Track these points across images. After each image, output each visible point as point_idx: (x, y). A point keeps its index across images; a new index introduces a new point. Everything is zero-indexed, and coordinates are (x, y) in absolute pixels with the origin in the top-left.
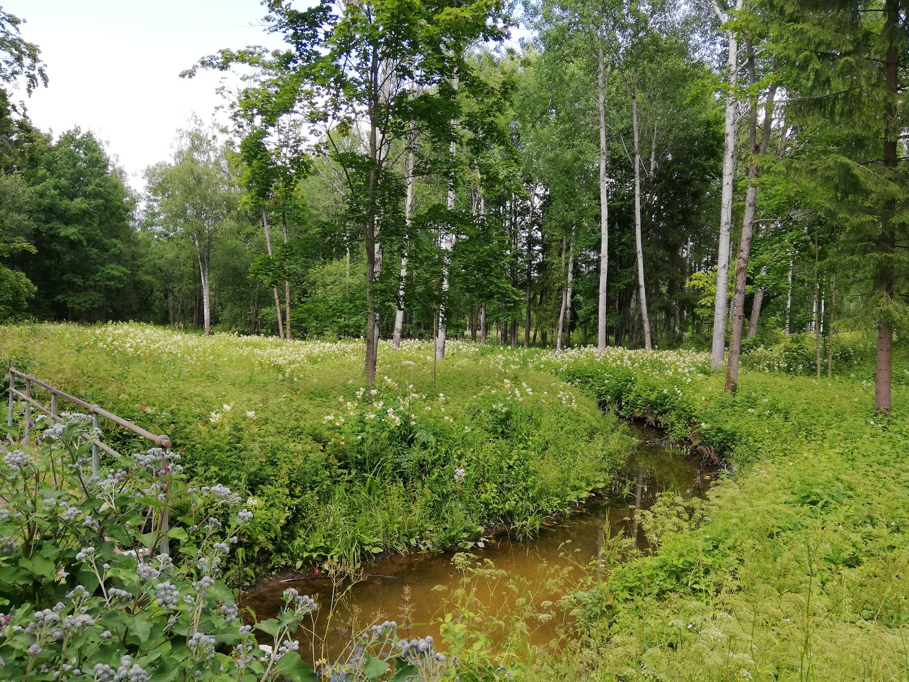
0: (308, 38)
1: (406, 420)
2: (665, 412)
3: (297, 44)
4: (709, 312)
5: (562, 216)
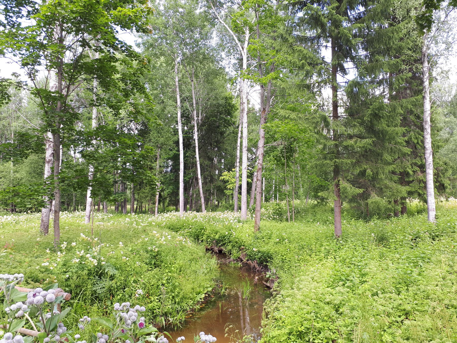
0: (14, 12)
1: (99, 261)
2: (224, 244)
3: (6, 15)
4: (231, 192)
5: (157, 140)
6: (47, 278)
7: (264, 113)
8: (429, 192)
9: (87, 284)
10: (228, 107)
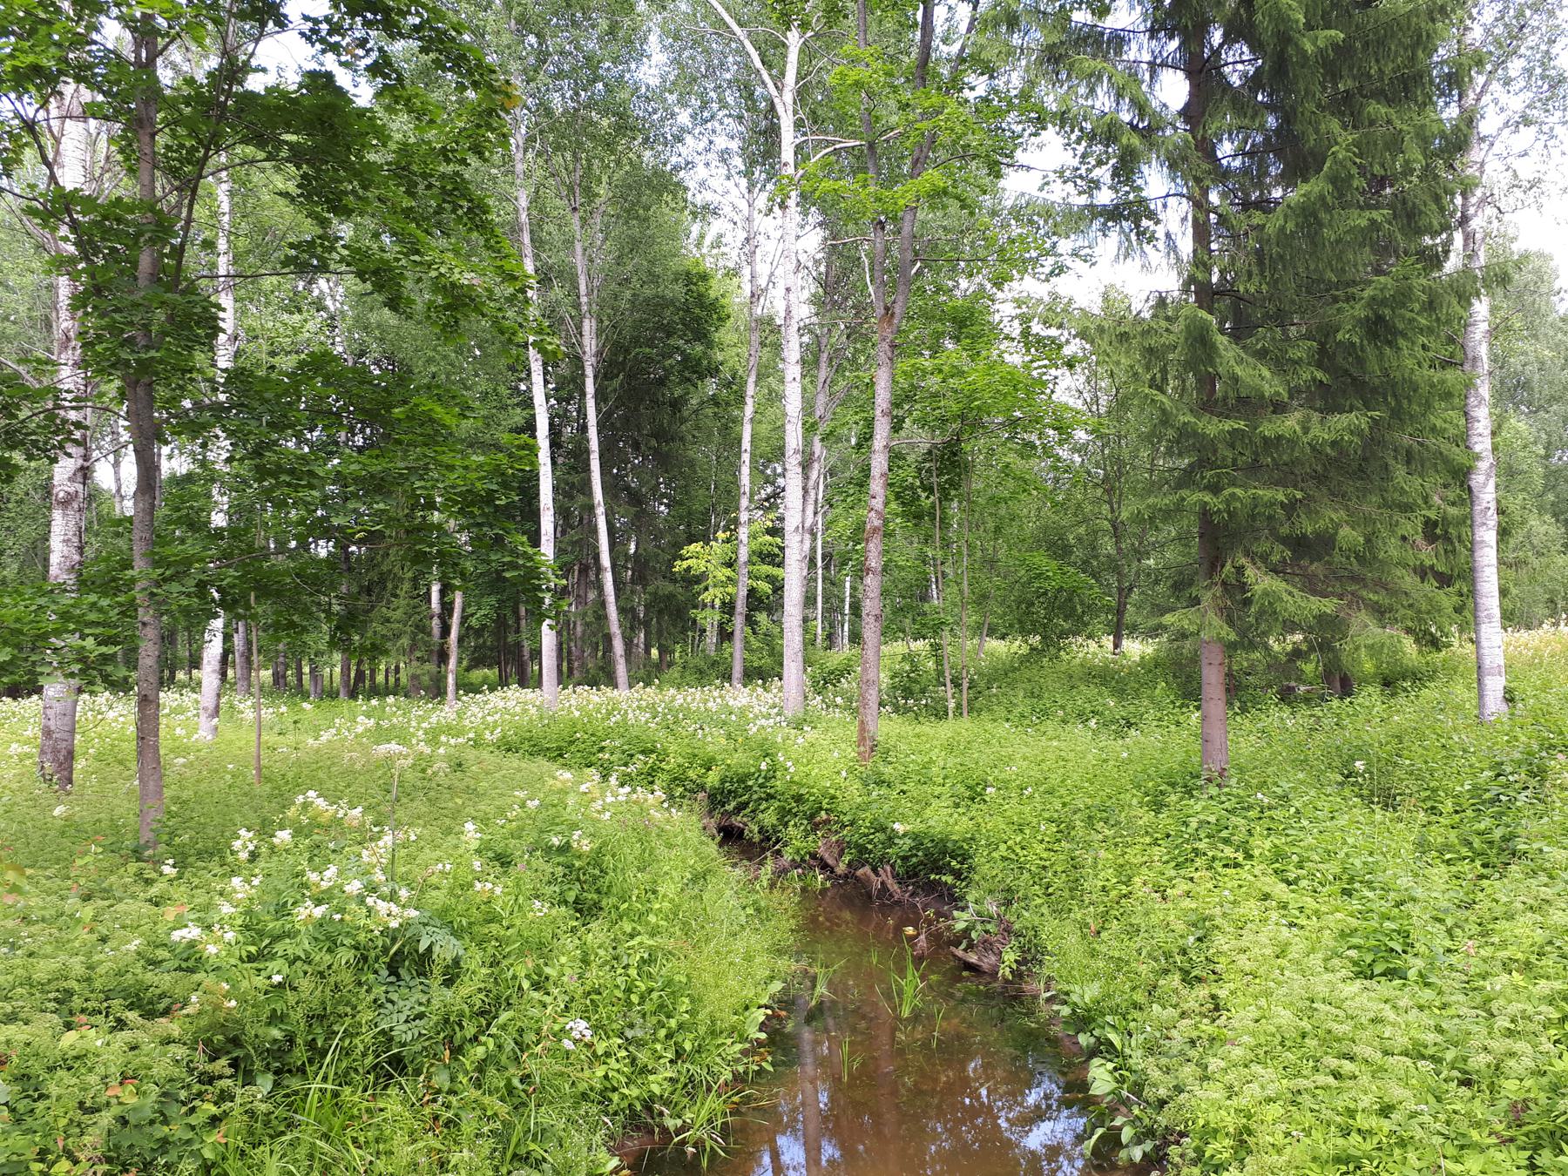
2: (744, 805)
7: (890, 323)
8: (1482, 608)
9: (354, 1008)
10: (697, 311)
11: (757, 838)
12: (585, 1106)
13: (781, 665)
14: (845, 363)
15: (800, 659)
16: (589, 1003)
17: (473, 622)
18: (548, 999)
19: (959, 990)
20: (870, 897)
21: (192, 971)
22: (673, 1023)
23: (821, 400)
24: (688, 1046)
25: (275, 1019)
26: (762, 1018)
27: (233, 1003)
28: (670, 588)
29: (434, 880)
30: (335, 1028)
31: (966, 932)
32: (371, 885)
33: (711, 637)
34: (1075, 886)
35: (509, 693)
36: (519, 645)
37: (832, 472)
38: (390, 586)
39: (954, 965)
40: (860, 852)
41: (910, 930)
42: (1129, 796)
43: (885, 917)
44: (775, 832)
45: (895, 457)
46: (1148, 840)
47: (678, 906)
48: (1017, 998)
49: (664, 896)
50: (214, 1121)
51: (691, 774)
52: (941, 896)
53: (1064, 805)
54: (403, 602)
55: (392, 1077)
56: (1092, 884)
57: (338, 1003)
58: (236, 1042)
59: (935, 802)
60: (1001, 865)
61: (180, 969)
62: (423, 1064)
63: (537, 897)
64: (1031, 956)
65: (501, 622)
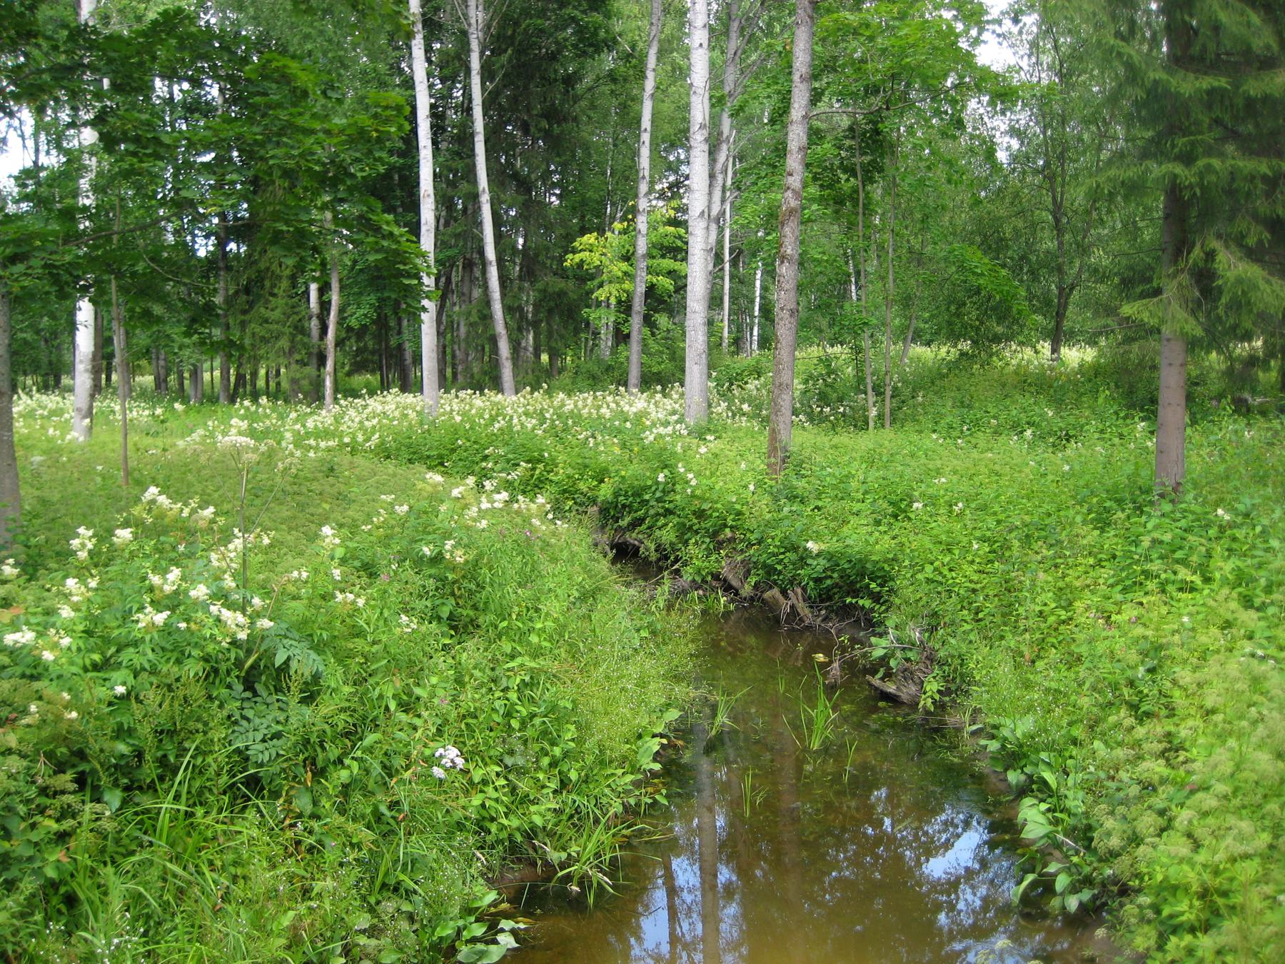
2: (641, 521)
6: (29, 700)
9: (206, 724)
11: (654, 557)
12: (459, 837)
13: (683, 371)
14: (759, 34)
15: (704, 361)
16: (461, 728)
17: (353, 323)
18: (417, 722)
19: (874, 722)
20: (777, 620)
21: (33, 678)
22: (557, 751)
23: (731, 77)
24: (573, 775)
25: (121, 733)
26: (656, 748)
27: (74, 715)
28: (560, 284)
29: (291, 589)
30: (186, 745)
31: (884, 660)
32: (217, 594)
33: (606, 340)
34: (1007, 611)
35: (389, 398)
36: (400, 348)
37: (741, 157)
38: (267, 284)
39: (870, 695)
40: (769, 573)
41: (820, 657)
42: (1071, 512)
43: (795, 643)
44: (674, 550)
45: (815, 136)
46: (1091, 561)
47: (564, 626)
48: (939, 730)
49: (547, 614)
50: (62, 837)
51: (582, 486)
52: (857, 621)
53: (999, 522)
54: (281, 302)
55: (250, 799)
56: (1027, 609)
57: (189, 718)
58: (81, 755)
59: (853, 520)
60: (926, 588)
61: (23, 676)
62: (282, 786)
63: (406, 611)
64: (957, 686)
65: (381, 322)
